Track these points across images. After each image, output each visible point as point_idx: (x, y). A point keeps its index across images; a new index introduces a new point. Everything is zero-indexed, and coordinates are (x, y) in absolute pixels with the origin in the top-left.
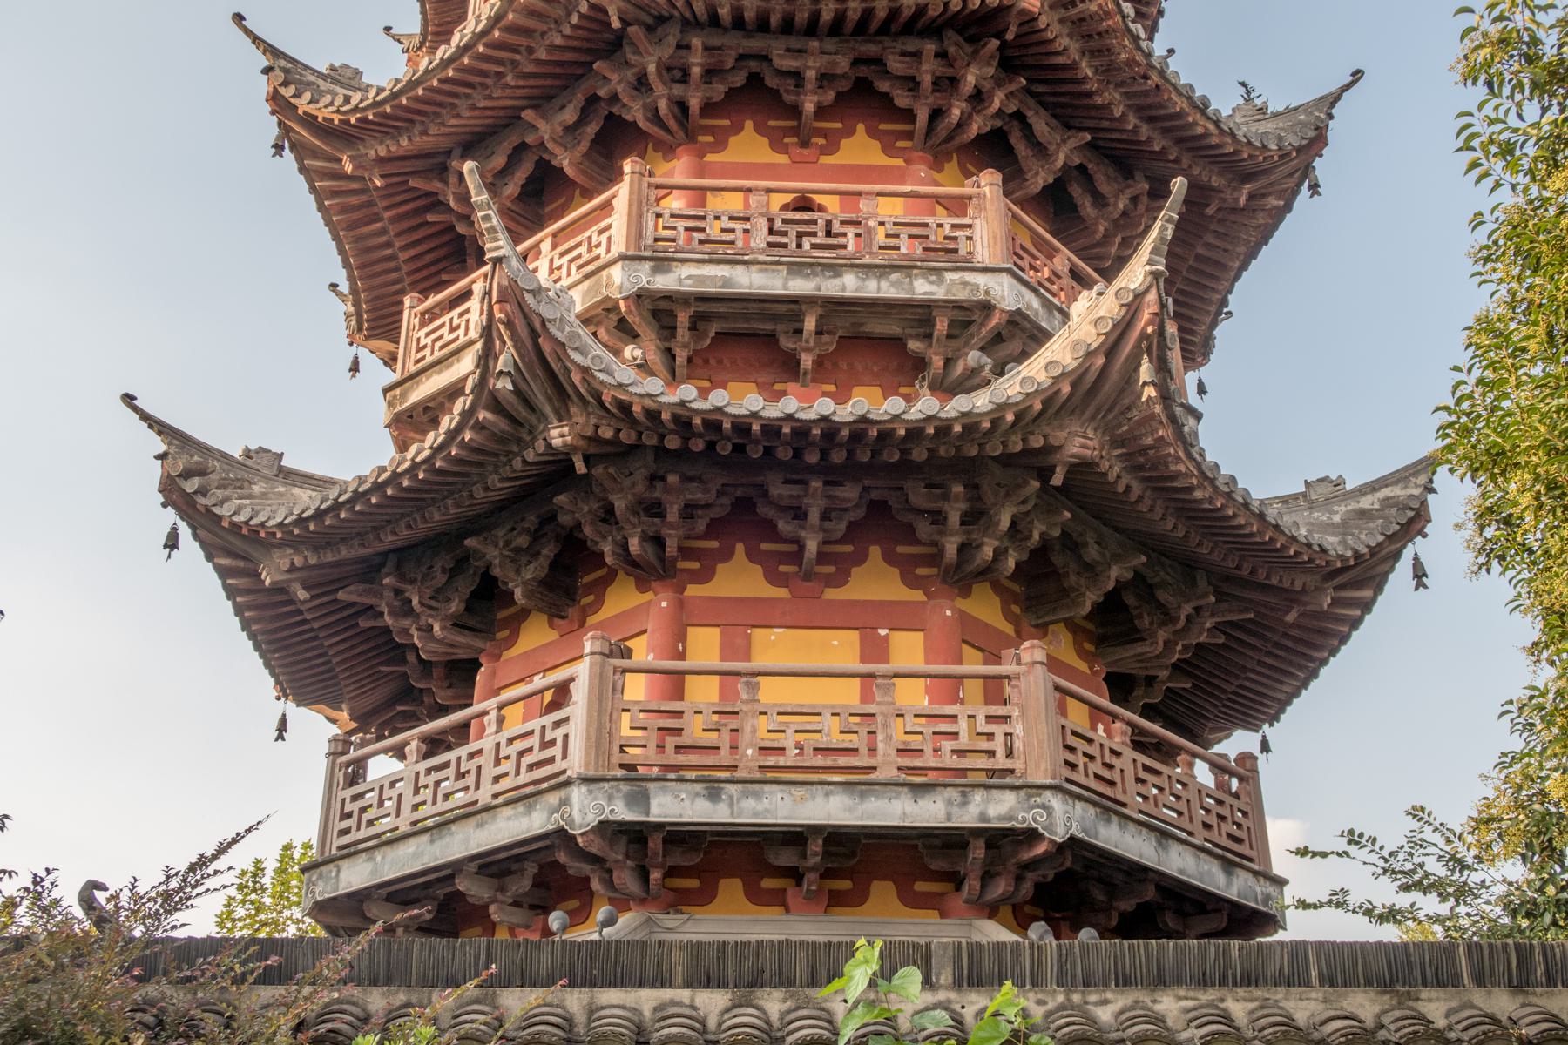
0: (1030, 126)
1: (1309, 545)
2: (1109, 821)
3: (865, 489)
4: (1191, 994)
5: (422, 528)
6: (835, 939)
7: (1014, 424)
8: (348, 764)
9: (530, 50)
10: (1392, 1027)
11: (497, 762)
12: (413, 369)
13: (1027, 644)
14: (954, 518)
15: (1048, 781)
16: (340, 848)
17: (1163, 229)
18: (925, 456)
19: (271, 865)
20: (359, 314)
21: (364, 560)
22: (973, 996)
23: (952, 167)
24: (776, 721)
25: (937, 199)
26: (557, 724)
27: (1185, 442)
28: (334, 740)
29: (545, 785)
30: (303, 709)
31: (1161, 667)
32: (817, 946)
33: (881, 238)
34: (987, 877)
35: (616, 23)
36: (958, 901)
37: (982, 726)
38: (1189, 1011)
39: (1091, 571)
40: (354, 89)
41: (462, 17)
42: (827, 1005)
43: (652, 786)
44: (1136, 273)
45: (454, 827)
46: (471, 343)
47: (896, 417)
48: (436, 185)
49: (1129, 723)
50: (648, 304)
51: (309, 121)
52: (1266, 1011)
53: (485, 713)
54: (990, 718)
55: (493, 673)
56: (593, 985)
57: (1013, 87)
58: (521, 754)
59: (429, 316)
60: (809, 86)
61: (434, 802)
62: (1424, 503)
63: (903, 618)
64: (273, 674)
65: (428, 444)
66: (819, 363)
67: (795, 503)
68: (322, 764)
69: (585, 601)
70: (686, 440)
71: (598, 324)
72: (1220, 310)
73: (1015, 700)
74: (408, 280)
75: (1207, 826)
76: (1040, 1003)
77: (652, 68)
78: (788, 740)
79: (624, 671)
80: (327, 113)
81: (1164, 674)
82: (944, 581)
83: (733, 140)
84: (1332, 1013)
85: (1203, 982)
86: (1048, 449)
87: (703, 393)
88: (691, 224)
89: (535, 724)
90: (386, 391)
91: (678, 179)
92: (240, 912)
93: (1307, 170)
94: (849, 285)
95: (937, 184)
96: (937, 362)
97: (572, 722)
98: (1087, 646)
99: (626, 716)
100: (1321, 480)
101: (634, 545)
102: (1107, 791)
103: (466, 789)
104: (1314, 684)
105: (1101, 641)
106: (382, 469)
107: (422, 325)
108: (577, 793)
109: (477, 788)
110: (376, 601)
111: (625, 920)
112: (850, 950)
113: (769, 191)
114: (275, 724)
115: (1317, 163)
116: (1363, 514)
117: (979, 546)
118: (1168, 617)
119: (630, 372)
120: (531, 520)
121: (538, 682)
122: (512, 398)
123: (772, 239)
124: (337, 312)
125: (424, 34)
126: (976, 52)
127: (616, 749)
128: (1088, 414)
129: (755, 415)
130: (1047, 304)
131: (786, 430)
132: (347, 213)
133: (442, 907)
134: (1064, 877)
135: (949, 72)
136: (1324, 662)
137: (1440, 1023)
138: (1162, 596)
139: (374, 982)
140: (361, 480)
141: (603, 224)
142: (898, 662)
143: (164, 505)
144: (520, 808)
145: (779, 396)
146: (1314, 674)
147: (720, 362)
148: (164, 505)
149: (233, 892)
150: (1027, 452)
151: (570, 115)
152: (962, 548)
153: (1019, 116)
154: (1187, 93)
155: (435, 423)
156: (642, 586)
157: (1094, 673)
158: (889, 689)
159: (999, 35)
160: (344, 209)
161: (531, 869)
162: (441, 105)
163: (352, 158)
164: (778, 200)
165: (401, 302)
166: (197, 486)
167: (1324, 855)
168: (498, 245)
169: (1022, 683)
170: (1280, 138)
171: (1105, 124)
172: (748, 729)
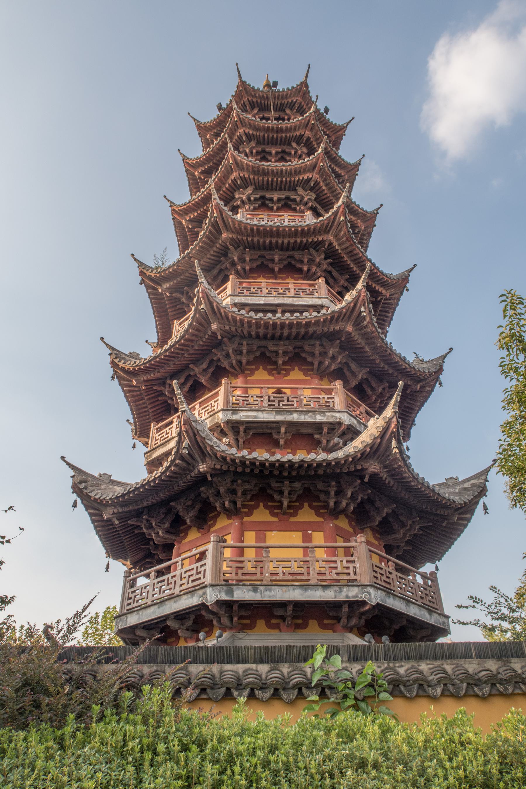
0: (350, 367)
1: (449, 500)
2: (390, 597)
3: (303, 484)
4: (432, 662)
5: (157, 499)
6: (306, 645)
7: (352, 461)
8: (131, 580)
9: (193, 346)
10: (503, 673)
11: (181, 579)
12: (154, 447)
13: (359, 535)
14: (332, 493)
15: (369, 583)
16: (127, 610)
17: (397, 398)
18: (323, 472)
19: (101, 615)
20: (136, 429)
21: (138, 510)
22: (355, 665)
23: (326, 380)
24: (276, 564)
25: (322, 390)
26: (201, 566)
27: (407, 466)
28: (126, 572)
29: (198, 587)
30: (115, 561)
31: (402, 542)
32: (299, 647)
33: (305, 402)
34: (349, 618)
35: (220, 338)
36: (339, 627)
37: (345, 565)
38: (431, 669)
39: (378, 510)
40: (137, 359)
41: (170, 337)
42: (304, 669)
43: (234, 587)
44: (389, 412)
45: (166, 603)
46: (173, 438)
47: (313, 460)
48: (162, 388)
49: (394, 562)
50: (230, 425)
51: (123, 369)
52: (458, 668)
53: (177, 562)
54: (348, 562)
55: (179, 548)
56: (222, 663)
57: (344, 355)
58: (189, 576)
59: (159, 430)
60: (280, 355)
61: (160, 594)
62: (485, 485)
63: (316, 527)
64: (105, 549)
65: (159, 471)
66: (286, 443)
67: (280, 489)
68: (122, 580)
69: (210, 523)
70: (244, 469)
71: (214, 431)
72: (413, 423)
73: (356, 554)
74: (152, 418)
75: (422, 598)
76: (379, 667)
77: (231, 351)
78: (280, 570)
79: (224, 547)
80: (129, 366)
81: (403, 545)
82: (329, 514)
83: (256, 372)
84: (481, 669)
85: (435, 658)
86: (363, 470)
87: (250, 453)
88: (244, 399)
89: (194, 566)
90: (145, 454)
91: (239, 385)
92: (90, 631)
93: (438, 379)
94: (295, 417)
95: (321, 385)
96: (324, 442)
97: (207, 565)
98: (377, 535)
99: (225, 563)
100: (451, 478)
101: (227, 504)
102: (388, 586)
103: (170, 589)
104: (453, 547)
105: (381, 534)
106: (144, 480)
107: (157, 432)
108: (209, 590)
109: (174, 588)
110: (140, 526)
111: (225, 635)
112: (313, 649)
113: (268, 388)
114: (105, 566)
115: (441, 376)
116: (465, 489)
117: (341, 502)
118: (403, 525)
119: (225, 446)
120: (192, 496)
121: (194, 551)
122: (187, 456)
123: (270, 403)
124: (129, 428)
125: (158, 343)
126: (332, 344)
127: (222, 574)
128: (376, 458)
129: (267, 460)
130: (359, 422)
131: (277, 465)
132: (134, 397)
133: (162, 631)
134: (375, 617)
135: (324, 350)
136: (456, 539)
137: (520, 671)
138: (402, 518)
139: (145, 662)
140: (137, 483)
141: (216, 399)
142: (315, 543)
143: (73, 493)
144: (189, 595)
145: (274, 454)
146: (453, 544)
147: (253, 443)
148: (73, 493)
149: (88, 624)
150: (356, 471)
151: (204, 366)
152: (335, 503)
153: (346, 363)
154: (399, 355)
155: (161, 465)
156: (229, 518)
157: (380, 545)
158: (313, 552)
159: (339, 339)
160: (133, 396)
161: (193, 617)
162: (164, 363)
163: (136, 380)
164: (271, 391)
165: (150, 425)
166: (84, 487)
167: (467, 607)
168: (183, 407)
169: (358, 549)
170: (429, 369)
171: (374, 366)
172: (266, 567)
